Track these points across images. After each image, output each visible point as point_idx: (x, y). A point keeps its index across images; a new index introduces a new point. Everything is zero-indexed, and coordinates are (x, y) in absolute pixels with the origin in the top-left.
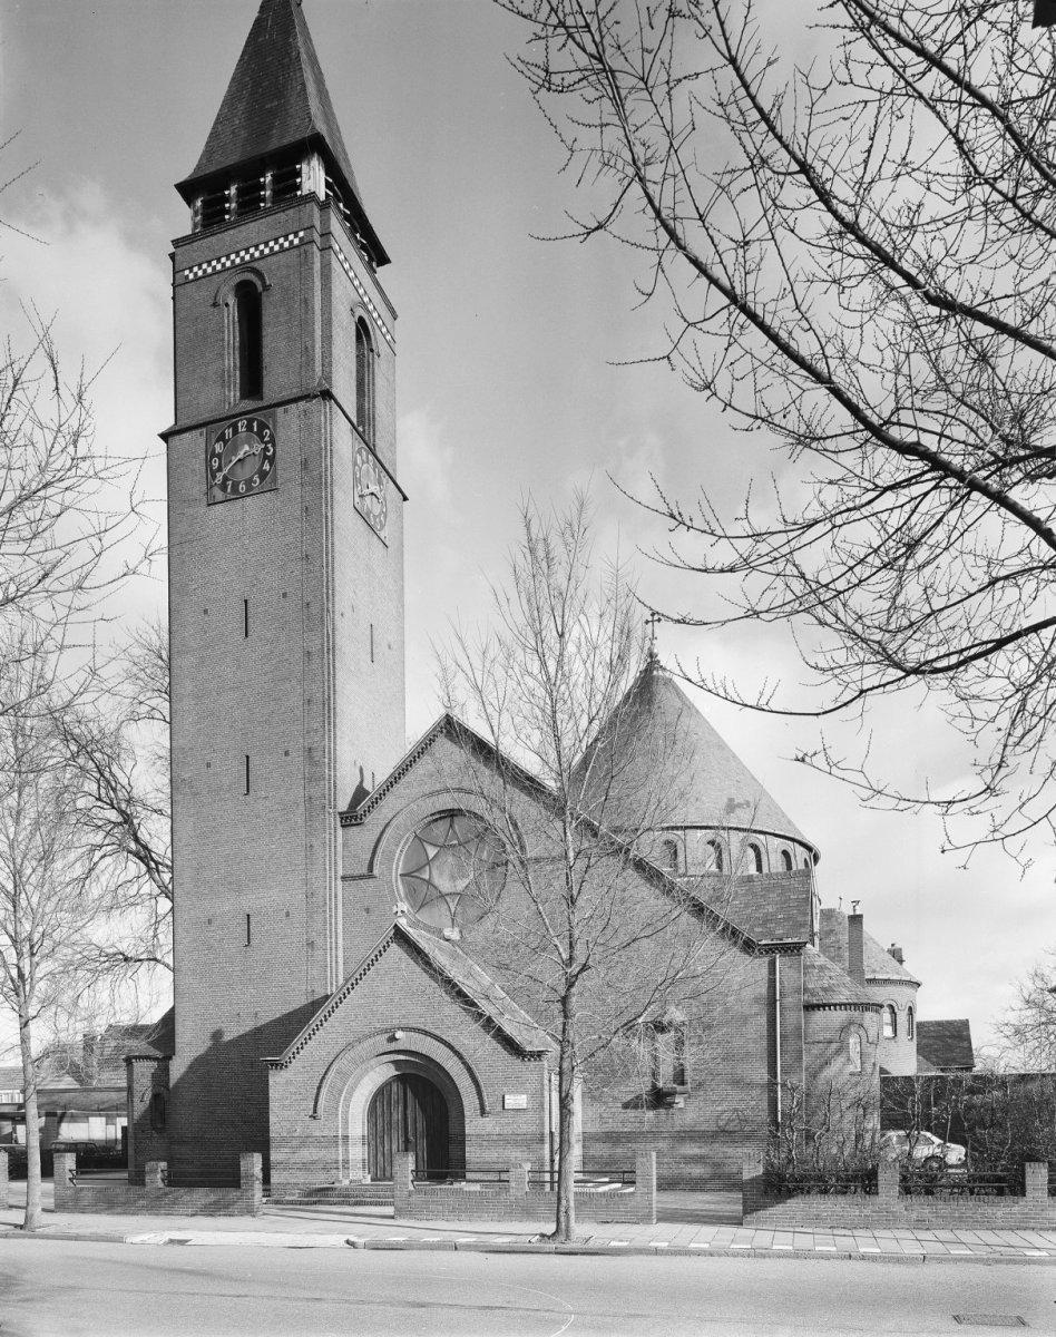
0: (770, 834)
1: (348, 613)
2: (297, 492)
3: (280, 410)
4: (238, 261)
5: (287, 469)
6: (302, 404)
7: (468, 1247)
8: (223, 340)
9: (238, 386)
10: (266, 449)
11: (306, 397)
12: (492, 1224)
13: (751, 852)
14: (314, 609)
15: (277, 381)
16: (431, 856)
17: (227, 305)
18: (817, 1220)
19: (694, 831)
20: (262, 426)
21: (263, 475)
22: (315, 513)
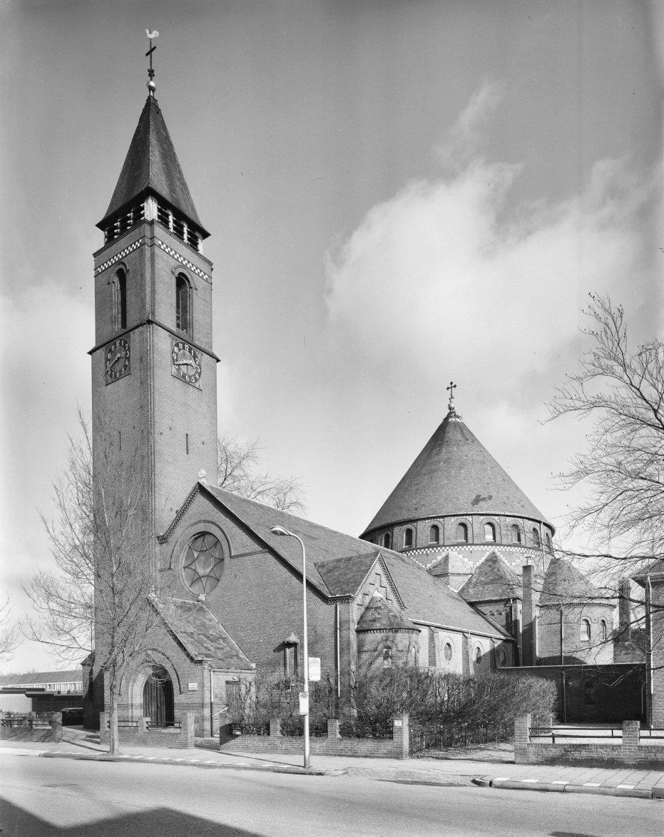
0: (502, 515)
1: (166, 431)
2: (138, 374)
3: (132, 333)
4: (117, 259)
5: (135, 364)
6: (140, 329)
7: (268, 770)
8: (112, 301)
9: (120, 322)
10: (126, 354)
11: (141, 325)
12: (283, 756)
13: (489, 528)
14: (145, 434)
15: (132, 319)
16: (196, 557)
17: (114, 282)
18: (246, 748)
19: (449, 518)
20: (125, 342)
21: (125, 367)
22: (145, 385)
